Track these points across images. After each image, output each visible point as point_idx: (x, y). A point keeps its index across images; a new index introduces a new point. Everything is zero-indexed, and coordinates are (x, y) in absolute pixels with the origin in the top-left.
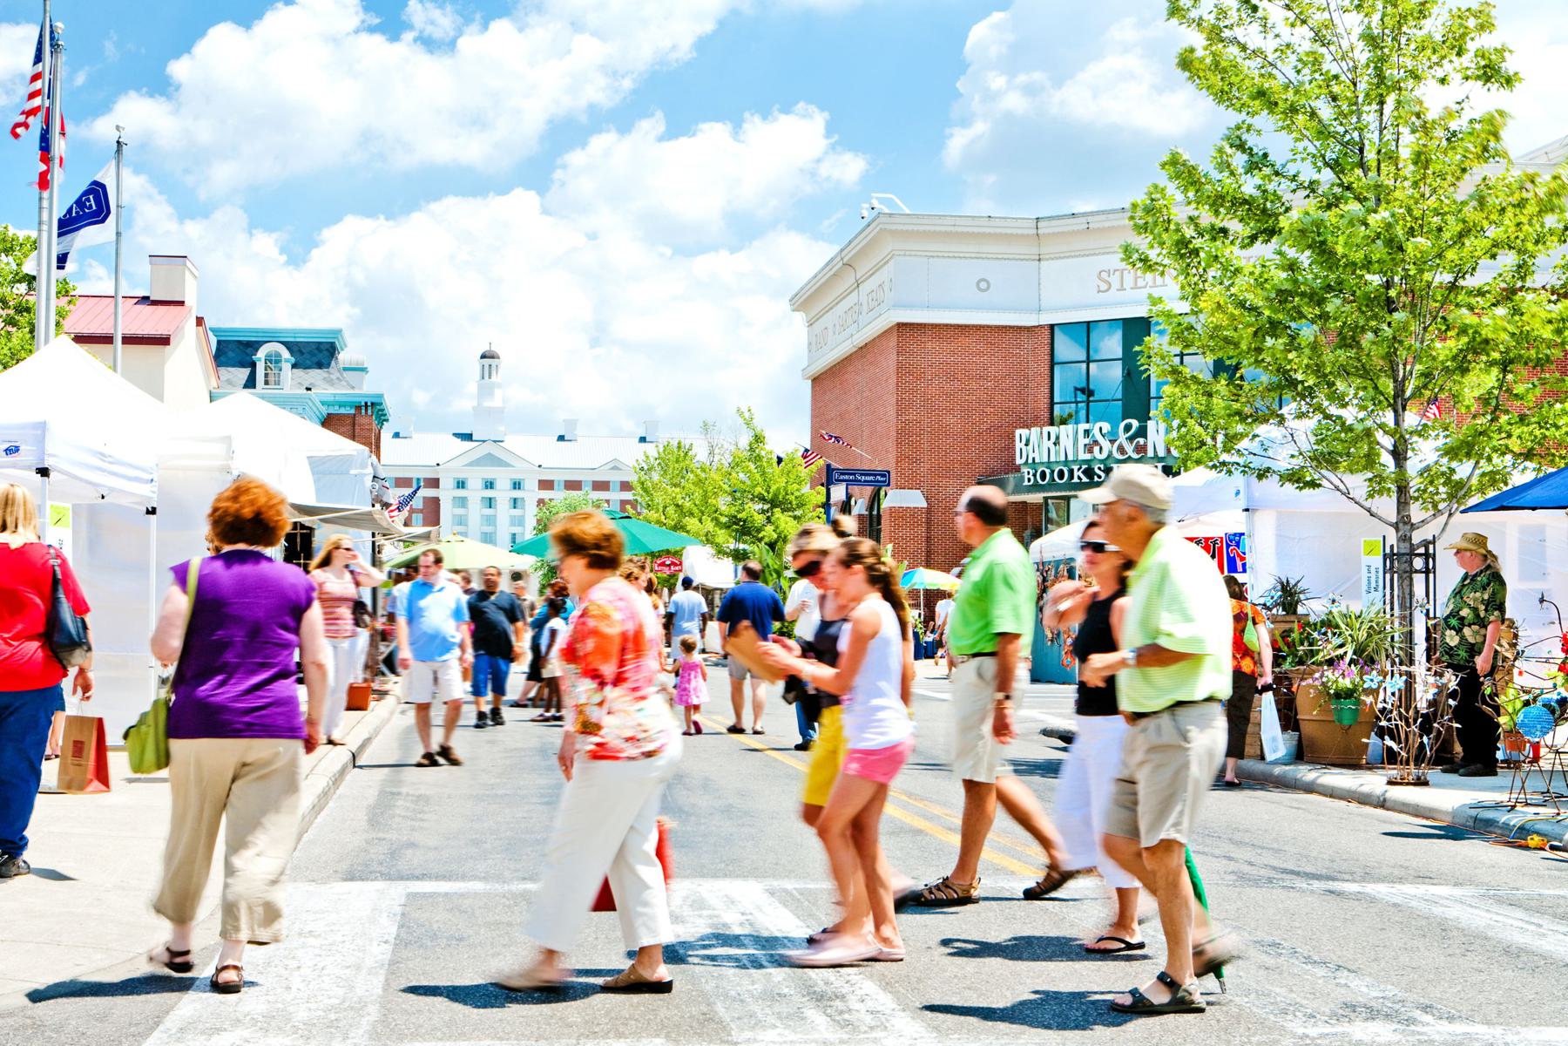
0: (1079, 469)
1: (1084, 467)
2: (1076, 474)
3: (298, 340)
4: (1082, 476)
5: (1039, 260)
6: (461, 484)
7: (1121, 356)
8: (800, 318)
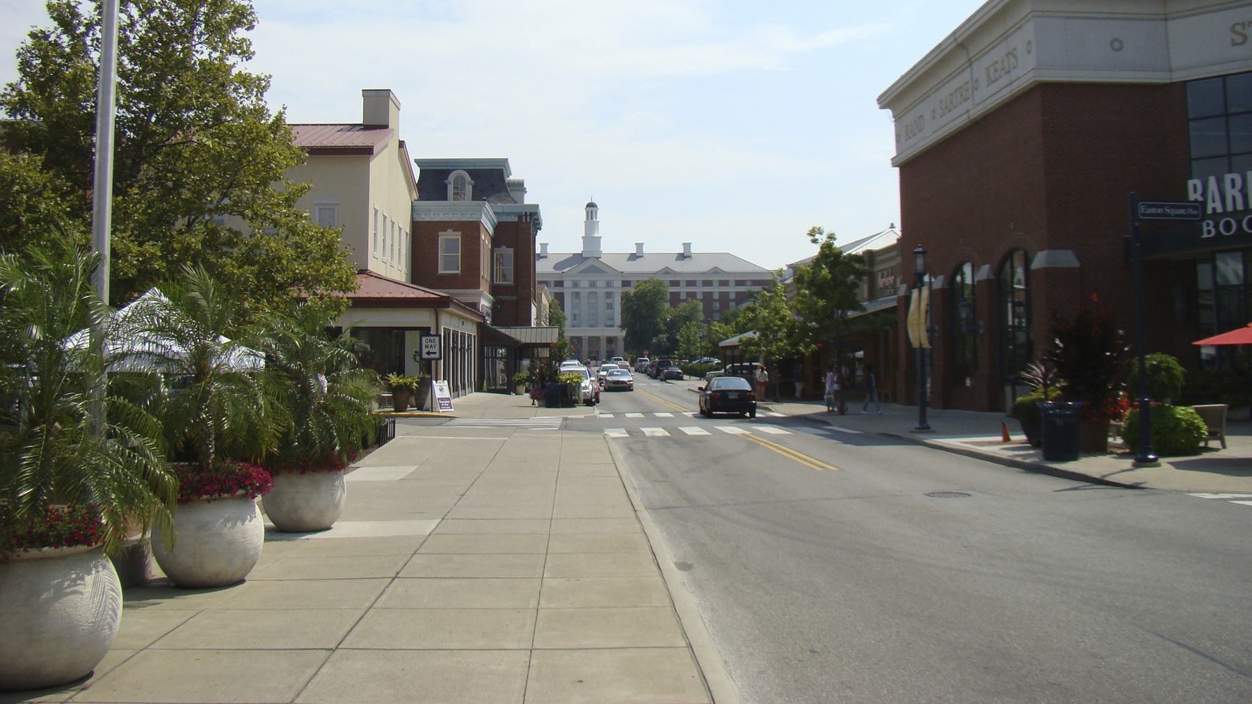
3: (477, 168)
6: (576, 284)
8: (888, 113)
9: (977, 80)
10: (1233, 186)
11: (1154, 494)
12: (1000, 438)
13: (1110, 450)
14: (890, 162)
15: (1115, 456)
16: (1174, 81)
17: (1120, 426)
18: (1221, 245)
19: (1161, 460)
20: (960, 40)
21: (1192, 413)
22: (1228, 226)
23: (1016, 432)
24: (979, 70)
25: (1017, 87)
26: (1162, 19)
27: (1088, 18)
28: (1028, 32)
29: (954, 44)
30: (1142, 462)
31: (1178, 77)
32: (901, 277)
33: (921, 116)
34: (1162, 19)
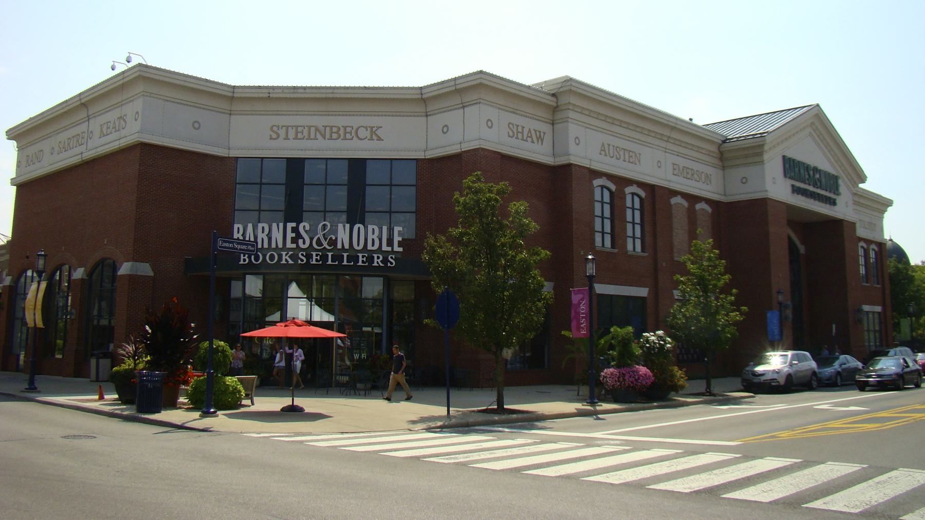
0: (286, 255)
1: (290, 253)
2: (284, 258)
4: (289, 260)
5: (230, 114)
7: (284, 182)
9: (92, 132)
10: (373, 233)
11: (220, 435)
12: (97, 397)
13: (178, 406)
14: (10, 181)
15: (184, 410)
16: (230, 156)
17: (188, 389)
18: (252, 269)
19: (218, 412)
20: (83, 101)
21: (235, 381)
22: (257, 259)
23: (110, 393)
24: (95, 124)
25: (123, 143)
26: (228, 114)
27: (181, 104)
28: (138, 105)
29: (79, 103)
30: (206, 414)
31: (233, 153)
32: (7, 270)
33: (42, 151)
34: (228, 114)
